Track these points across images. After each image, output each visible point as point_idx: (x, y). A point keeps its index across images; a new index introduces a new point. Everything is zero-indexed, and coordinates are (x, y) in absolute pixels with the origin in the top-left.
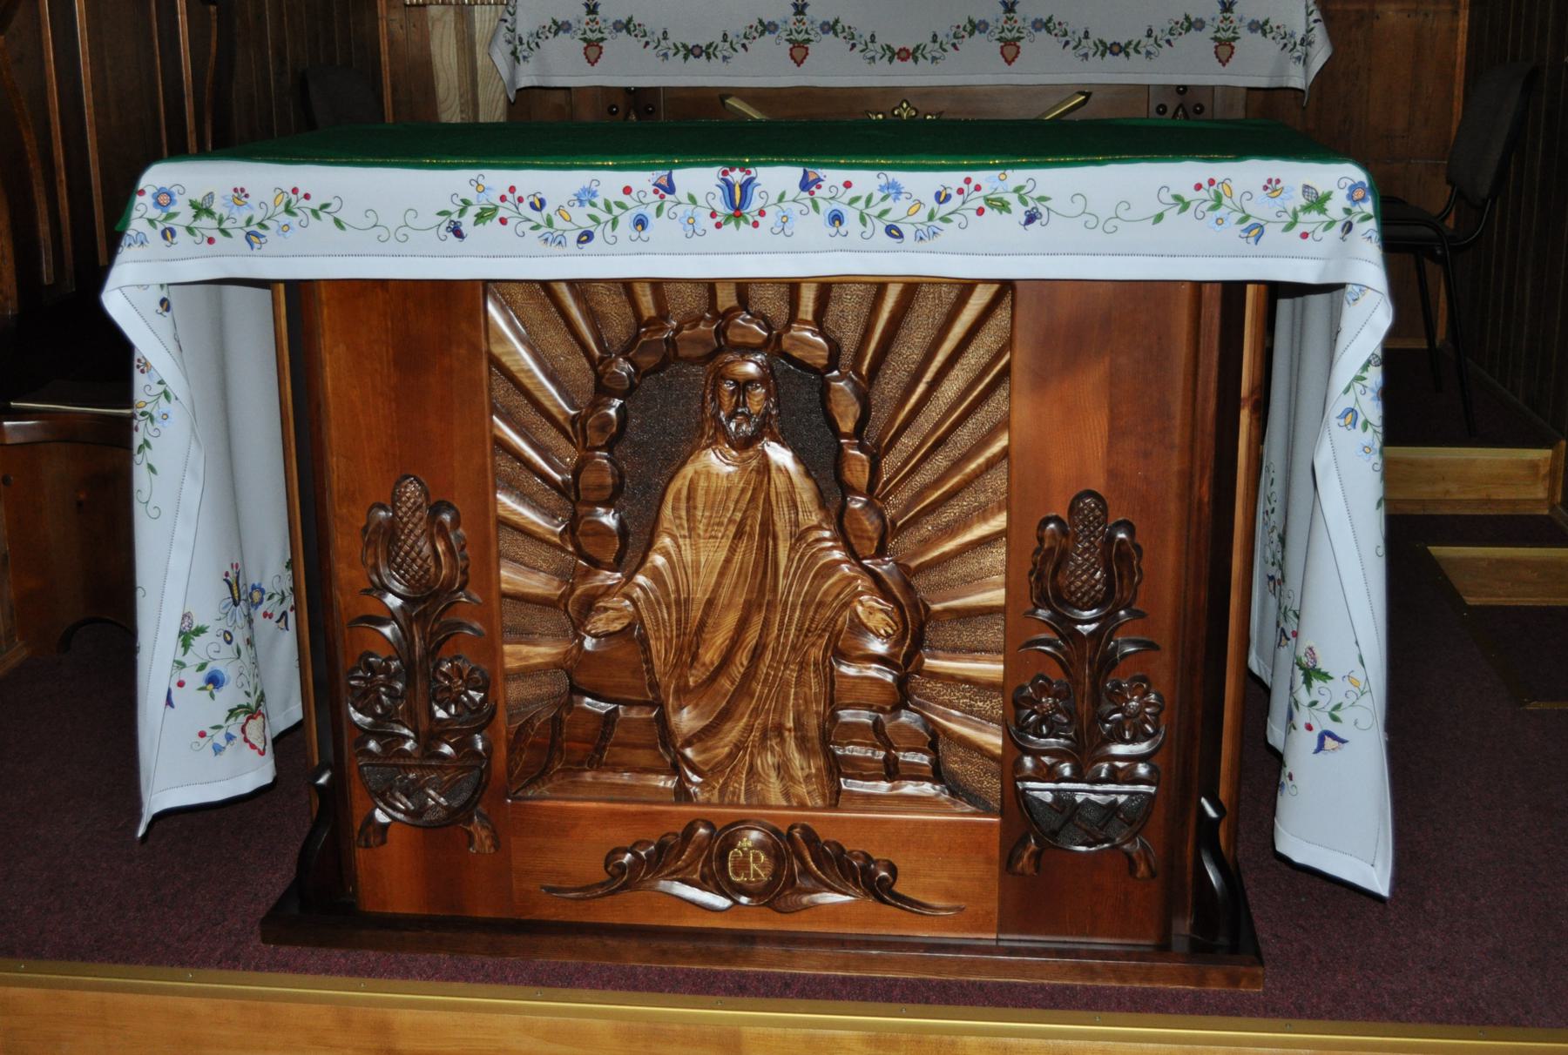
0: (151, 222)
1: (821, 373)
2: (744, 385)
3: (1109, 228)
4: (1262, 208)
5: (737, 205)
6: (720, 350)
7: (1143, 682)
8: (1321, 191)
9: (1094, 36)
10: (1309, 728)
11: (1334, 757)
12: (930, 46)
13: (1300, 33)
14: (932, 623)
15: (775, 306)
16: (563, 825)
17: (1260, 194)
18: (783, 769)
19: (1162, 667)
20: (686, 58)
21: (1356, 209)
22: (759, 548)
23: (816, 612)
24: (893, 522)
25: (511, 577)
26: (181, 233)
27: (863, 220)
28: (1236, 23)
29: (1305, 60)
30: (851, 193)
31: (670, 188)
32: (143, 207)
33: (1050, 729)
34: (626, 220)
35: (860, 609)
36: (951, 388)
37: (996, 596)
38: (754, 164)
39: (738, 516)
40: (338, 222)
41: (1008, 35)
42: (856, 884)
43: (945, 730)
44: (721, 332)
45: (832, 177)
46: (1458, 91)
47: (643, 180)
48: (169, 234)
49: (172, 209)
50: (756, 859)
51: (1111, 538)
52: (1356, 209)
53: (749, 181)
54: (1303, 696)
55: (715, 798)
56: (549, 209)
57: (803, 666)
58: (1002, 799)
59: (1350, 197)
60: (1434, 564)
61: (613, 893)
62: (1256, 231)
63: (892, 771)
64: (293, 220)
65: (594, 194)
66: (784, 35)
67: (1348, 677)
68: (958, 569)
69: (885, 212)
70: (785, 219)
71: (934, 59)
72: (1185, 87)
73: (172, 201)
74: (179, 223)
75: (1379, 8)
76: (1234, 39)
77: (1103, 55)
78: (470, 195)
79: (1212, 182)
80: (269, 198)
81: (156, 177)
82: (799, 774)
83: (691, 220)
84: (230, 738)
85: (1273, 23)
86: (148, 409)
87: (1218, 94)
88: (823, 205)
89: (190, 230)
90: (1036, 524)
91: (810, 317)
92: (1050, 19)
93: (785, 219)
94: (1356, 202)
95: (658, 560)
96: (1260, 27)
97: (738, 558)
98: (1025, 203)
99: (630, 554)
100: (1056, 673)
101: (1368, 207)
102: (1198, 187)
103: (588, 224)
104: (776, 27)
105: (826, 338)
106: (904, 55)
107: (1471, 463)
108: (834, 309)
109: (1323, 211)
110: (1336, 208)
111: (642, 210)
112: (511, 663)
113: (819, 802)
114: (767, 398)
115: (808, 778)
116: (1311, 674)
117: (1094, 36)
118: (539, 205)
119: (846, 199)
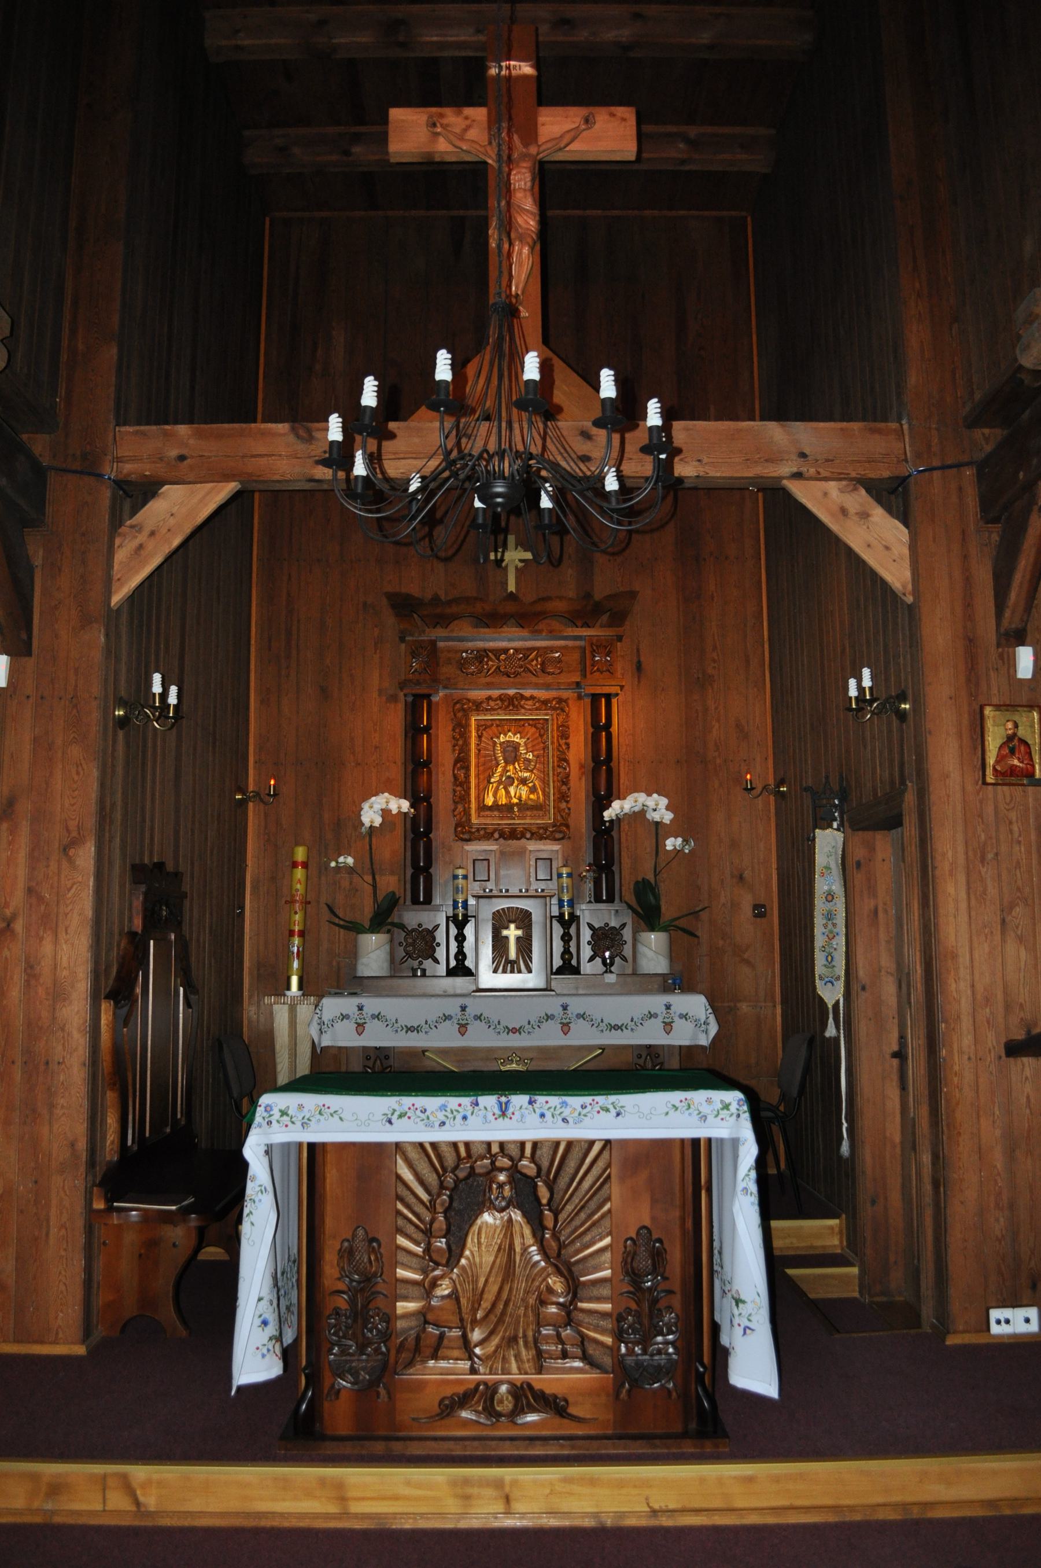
0: (264, 1118)
1: (532, 1179)
2: (501, 1186)
3: (648, 1117)
4: (706, 1109)
5: (503, 1111)
6: (492, 1170)
7: (670, 1308)
8: (727, 1102)
9: (606, 1021)
10: (739, 1325)
11: (751, 1337)
12: (527, 1026)
13: (703, 1019)
14: (581, 1287)
15: (515, 1152)
16: (421, 1385)
17: (704, 1104)
18: (518, 1357)
19: (676, 1301)
20: (407, 1032)
21: (741, 1109)
22: (508, 1255)
23: (532, 1283)
24: (564, 1242)
25: (402, 1273)
26: (274, 1123)
27: (553, 1117)
28: (673, 1015)
29: (706, 1032)
30: (548, 1105)
31: (477, 1104)
32: (260, 1111)
33: (633, 1330)
34: (459, 1117)
35: (550, 1281)
36: (586, 1184)
37: (607, 1273)
38: (510, 1094)
39: (499, 1241)
40: (341, 1119)
41: (564, 1021)
42: (551, 1409)
43: (587, 1335)
44: (493, 1163)
45: (541, 1099)
46: (780, 1045)
47: (466, 1101)
48: (270, 1123)
49: (271, 1113)
50: (507, 1398)
51: (654, 1246)
52: (741, 1109)
53: (508, 1101)
54: (736, 1312)
55: (488, 1371)
56: (428, 1113)
57: (526, 1308)
58: (613, 1367)
59: (738, 1104)
60: (789, 1279)
61: (442, 1419)
62: (704, 1118)
63: (565, 1355)
64: (322, 1118)
65: (446, 1106)
66: (456, 1021)
67: (753, 1301)
68: (592, 1262)
69: (561, 1113)
70: (522, 1116)
71: (529, 1032)
72: (650, 1046)
73: (271, 1110)
74: (274, 1119)
75: (739, 1005)
76: (672, 1022)
77: (610, 1030)
78: (396, 1107)
79: (686, 1099)
80: (313, 1108)
81: (266, 1099)
82: (525, 1358)
83: (485, 1117)
84: (269, 1350)
85: (690, 1015)
86: (253, 1197)
87: (666, 1049)
88: (537, 1110)
89: (278, 1122)
90: (623, 1240)
91: (529, 1156)
92: (584, 1014)
93: (522, 1116)
94: (740, 1106)
95: (463, 1261)
96: (684, 1017)
97: (498, 1260)
98: (615, 1108)
99: (452, 1259)
100: (633, 1306)
101: (745, 1108)
102: (681, 1101)
103: (443, 1119)
104: (452, 1017)
105: (536, 1164)
106: (514, 1031)
107: (801, 1227)
108: (538, 1153)
109: (728, 1109)
110: (733, 1108)
111: (465, 1113)
112: (399, 1311)
113: (533, 1371)
114: (511, 1190)
115: (528, 1361)
116: (738, 1301)
117: (606, 1021)
118: (424, 1111)
119: (547, 1107)
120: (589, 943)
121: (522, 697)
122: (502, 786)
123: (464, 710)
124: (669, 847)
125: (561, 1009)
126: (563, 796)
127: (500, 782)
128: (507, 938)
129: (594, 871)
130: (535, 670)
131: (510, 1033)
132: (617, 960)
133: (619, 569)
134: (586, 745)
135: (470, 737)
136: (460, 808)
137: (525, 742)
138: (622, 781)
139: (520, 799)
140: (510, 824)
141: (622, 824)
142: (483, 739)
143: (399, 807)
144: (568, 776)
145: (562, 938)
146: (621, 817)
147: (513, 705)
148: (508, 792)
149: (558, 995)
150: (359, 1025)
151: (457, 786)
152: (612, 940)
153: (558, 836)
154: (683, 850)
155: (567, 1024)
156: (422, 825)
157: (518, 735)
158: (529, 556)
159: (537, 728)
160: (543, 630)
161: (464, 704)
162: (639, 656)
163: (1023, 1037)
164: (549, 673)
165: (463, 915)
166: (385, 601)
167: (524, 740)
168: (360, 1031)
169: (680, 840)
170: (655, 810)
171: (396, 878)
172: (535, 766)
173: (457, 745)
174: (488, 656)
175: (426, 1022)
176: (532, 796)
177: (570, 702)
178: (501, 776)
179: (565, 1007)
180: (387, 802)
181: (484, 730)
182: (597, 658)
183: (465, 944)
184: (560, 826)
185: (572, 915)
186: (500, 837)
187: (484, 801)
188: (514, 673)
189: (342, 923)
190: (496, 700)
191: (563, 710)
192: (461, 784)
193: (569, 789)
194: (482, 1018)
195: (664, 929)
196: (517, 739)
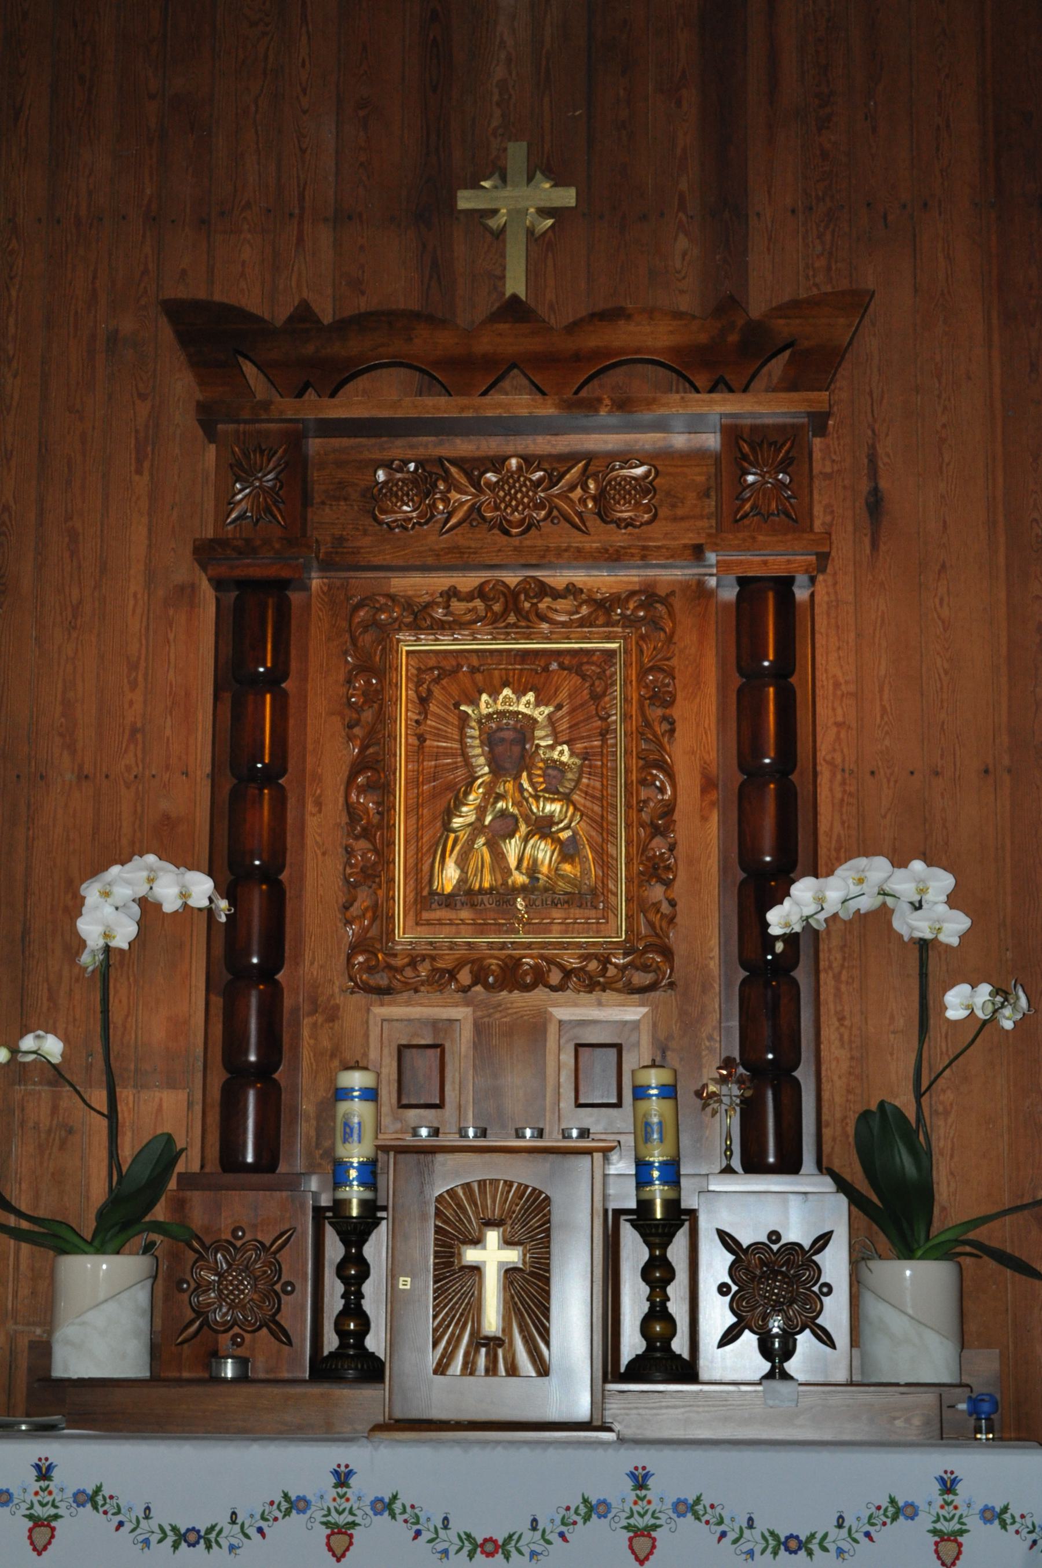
9: (762, 1525)
12: (528, 1536)
20: (176, 1546)
66: (319, 1516)
71: (533, 1554)
85: (1015, 1510)
104: (308, 1503)
117: (762, 1525)
120: (828, 1289)
121: (544, 590)
122: (481, 840)
123: (376, 623)
124: (955, 1013)
125: (630, 1483)
126: (655, 868)
127: (477, 828)
128: (476, 1270)
129: (740, 1081)
130: (580, 515)
131: (479, 1556)
132: (805, 1340)
133: (820, 236)
134: (722, 720)
135: (396, 701)
136: (363, 900)
137: (550, 716)
138: (823, 826)
139: (533, 872)
140: (503, 946)
141: (823, 946)
142: (433, 707)
143: (184, 895)
144: (668, 810)
145: (646, 1274)
146: (821, 927)
147: (518, 611)
148: (498, 857)
149: (621, 1440)
150: (38, 1522)
151: (357, 838)
152: (791, 1281)
153: (640, 978)
154: (993, 1019)
155: (646, 1532)
156: (255, 947)
157: (531, 696)
158: (567, 197)
159: (584, 677)
160: (600, 400)
161: (380, 610)
162: (873, 473)
163: (222, 1000)
164: (619, 523)
165: (363, 1204)
166: (167, 333)
167: (547, 710)
168: (40, 1540)
169: (985, 990)
170: (918, 906)
171: (182, 1096)
172: (578, 781)
173: (358, 723)
174: (447, 477)
175: (234, 1517)
176: (567, 867)
177: (677, 603)
178: (481, 811)
179: (640, 1481)
180: (151, 880)
181: (437, 680)
182: (750, 478)
183: (367, 1288)
184: (647, 949)
185: (673, 1206)
186: (475, 983)
187: (431, 882)
188: (521, 522)
189: (25, 1225)
190: (470, 597)
191: (655, 624)
192: (366, 834)
193: (672, 848)
194: (397, 1507)
195: (943, 1252)
196: (525, 704)
